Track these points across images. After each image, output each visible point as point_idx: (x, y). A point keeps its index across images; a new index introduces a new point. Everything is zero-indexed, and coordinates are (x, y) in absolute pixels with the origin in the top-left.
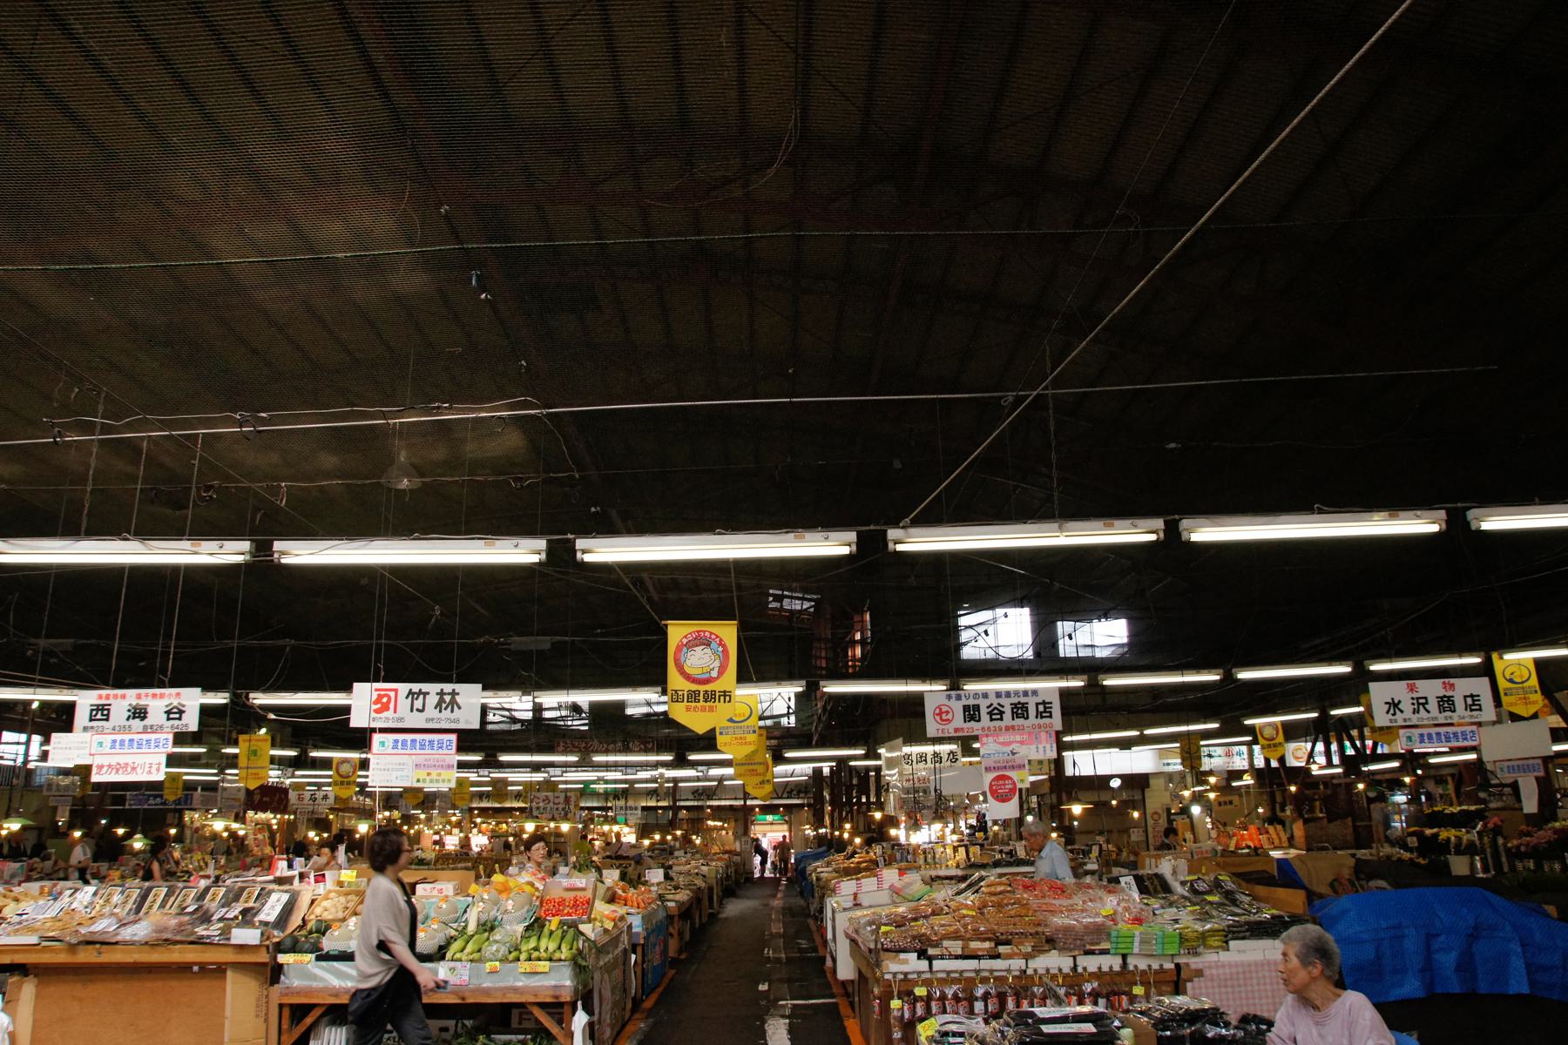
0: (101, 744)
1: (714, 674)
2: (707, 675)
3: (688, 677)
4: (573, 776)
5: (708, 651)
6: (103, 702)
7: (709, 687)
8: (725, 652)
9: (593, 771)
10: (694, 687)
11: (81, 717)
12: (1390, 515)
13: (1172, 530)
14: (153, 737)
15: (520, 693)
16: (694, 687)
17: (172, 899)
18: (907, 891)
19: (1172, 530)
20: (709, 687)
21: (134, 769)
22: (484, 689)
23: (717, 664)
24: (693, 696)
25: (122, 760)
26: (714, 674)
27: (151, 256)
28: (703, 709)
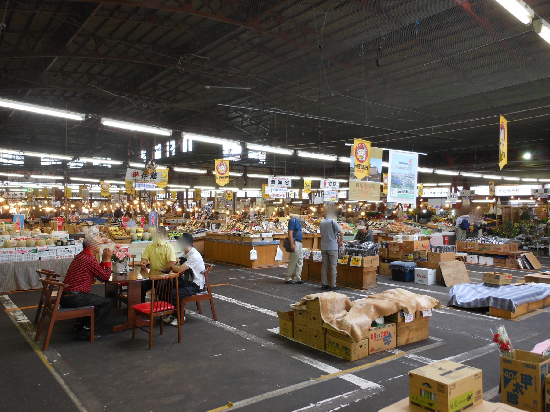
0: (274, 189)
1: (225, 172)
2: (223, 173)
3: (219, 173)
4: (16, 184)
5: (223, 166)
6: (273, 180)
7: (224, 175)
8: (227, 167)
9: (44, 184)
10: (221, 175)
11: (269, 182)
12: (158, 129)
13: (295, 153)
14: (284, 188)
15: (20, 151)
16: (221, 175)
17: (268, 236)
18: (163, 263)
19: (295, 153)
20: (224, 175)
21: (280, 196)
22: (417, 197)
23: (225, 170)
24: (220, 177)
25: (278, 193)
26: (225, 172)
27: (49, 71)
28: (222, 181)
